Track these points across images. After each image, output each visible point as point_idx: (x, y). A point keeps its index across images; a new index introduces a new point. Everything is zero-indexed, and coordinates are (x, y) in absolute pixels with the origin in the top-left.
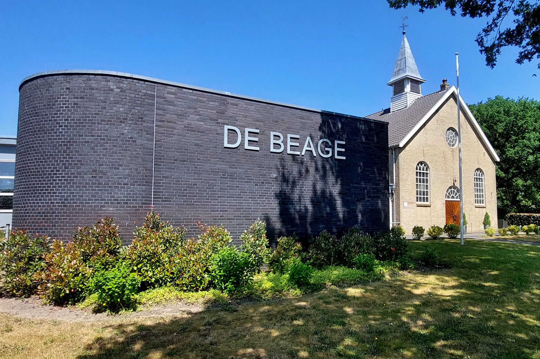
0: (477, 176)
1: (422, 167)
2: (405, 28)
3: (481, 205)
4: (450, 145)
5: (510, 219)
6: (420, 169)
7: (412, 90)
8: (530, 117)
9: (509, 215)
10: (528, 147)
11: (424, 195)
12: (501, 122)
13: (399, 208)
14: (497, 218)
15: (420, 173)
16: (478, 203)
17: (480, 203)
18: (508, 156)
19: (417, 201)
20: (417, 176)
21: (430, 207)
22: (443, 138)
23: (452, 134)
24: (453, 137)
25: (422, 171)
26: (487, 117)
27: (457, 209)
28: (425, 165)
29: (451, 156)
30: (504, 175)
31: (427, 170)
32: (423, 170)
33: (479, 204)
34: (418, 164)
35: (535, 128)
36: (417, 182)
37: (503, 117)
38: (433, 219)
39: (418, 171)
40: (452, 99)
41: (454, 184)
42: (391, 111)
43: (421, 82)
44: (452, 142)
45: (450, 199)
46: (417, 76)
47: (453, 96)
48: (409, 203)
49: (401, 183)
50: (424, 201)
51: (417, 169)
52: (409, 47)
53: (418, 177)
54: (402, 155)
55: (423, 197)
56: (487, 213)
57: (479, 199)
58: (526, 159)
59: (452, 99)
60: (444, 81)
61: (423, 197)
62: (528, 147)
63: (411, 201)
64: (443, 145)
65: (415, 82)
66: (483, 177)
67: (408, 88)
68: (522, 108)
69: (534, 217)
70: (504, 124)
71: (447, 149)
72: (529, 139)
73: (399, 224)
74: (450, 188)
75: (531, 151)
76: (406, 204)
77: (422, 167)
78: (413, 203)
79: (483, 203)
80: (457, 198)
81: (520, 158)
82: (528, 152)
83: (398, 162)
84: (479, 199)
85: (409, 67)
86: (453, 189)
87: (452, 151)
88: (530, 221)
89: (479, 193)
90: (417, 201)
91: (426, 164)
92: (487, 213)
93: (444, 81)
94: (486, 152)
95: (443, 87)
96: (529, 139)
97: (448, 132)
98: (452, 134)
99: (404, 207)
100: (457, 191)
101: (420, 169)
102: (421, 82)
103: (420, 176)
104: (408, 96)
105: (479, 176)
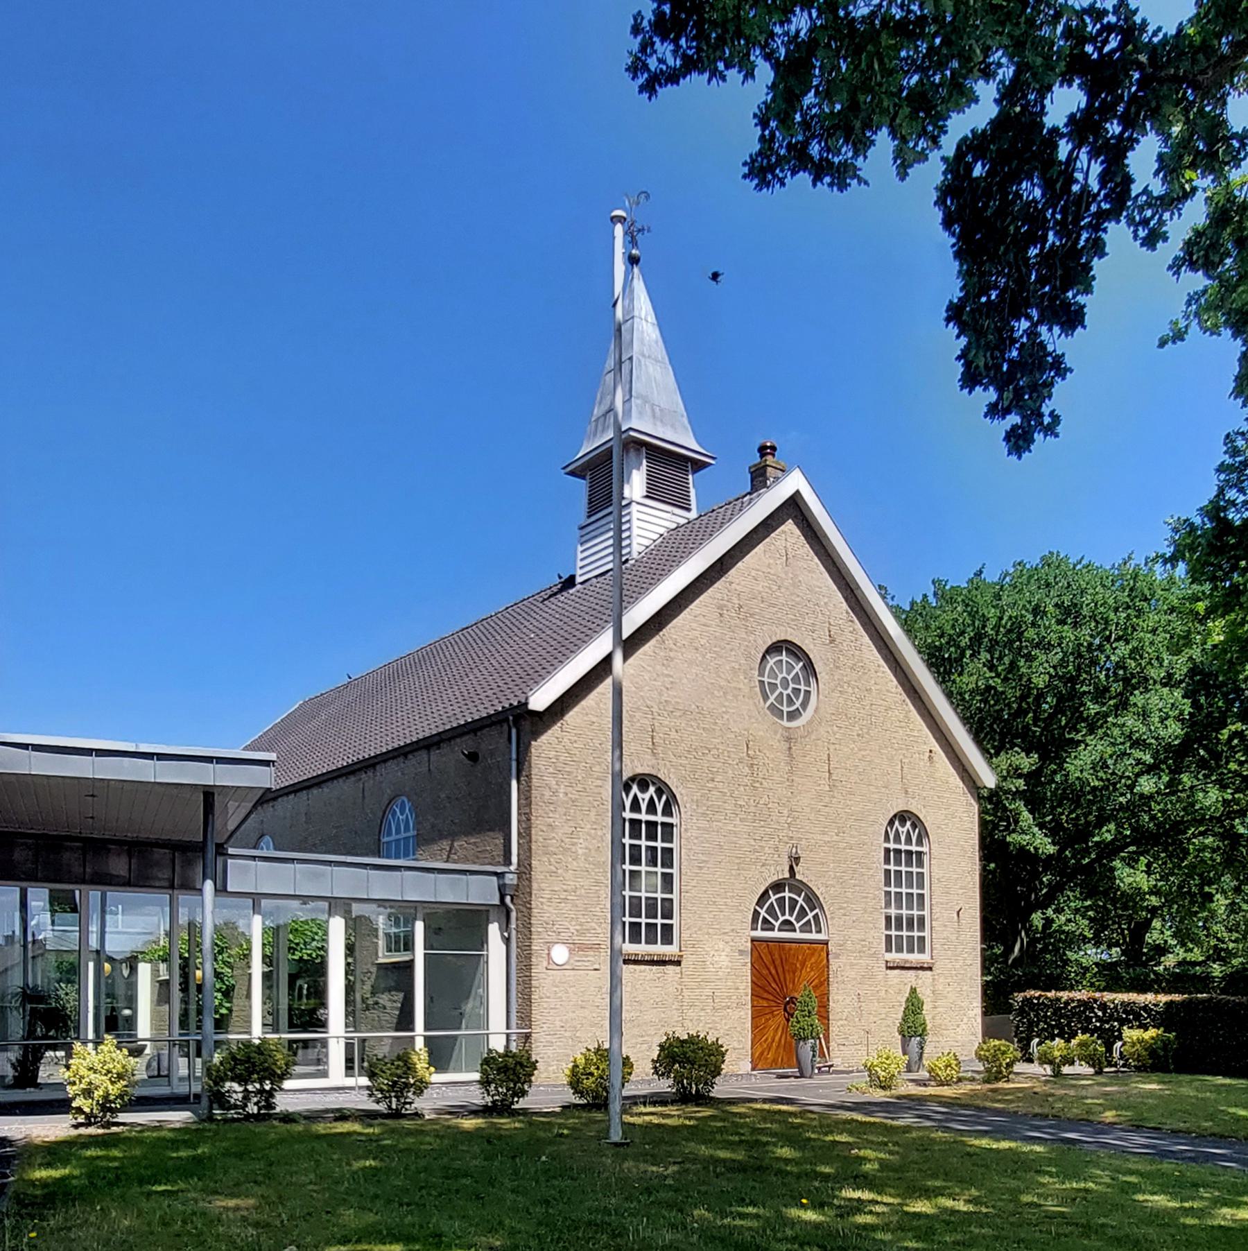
0: (897, 839)
1: (644, 798)
2: (639, 237)
3: (915, 958)
4: (775, 711)
5: (1021, 1012)
6: (897, 839)
7: (653, 493)
8: (1154, 631)
9: (1019, 997)
10: (1138, 743)
11: (652, 914)
12: (1048, 647)
13: (529, 967)
14: (978, 1011)
15: (898, 852)
16: (900, 950)
17: (911, 950)
18: (1071, 779)
19: (889, 950)
20: (887, 861)
21: (678, 963)
22: (747, 684)
23: (790, 668)
24: (796, 679)
25: (645, 819)
26: (996, 628)
27: (807, 975)
28: (659, 792)
29: (783, 757)
30: (1051, 849)
31: (919, 843)
32: (651, 808)
33: (905, 956)
34: (891, 823)
35: (1170, 676)
36: (888, 883)
37: (1051, 629)
38: (690, 1013)
39: (892, 846)
40: (790, 526)
41: (791, 869)
42: (579, 580)
43: (698, 466)
44: (790, 702)
45: (776, 934)
46: (684, 439)
47: (794, 508)
48: (577, 948)
49: (539, 865)
50: (651, 940)
51: (887, 839)
52: (652, 318)
53: (892, 867)
54: (545, 747)
55: (646, 924)
56: (913, 991)
57: (906, 930)
58: (1131, 788)
59: (790, 526)
60: (763, 450)
61: (646, 924)
62: (1138, 743)
63: (588, 939)
64: (748, 715)
65: (670, 468)
66: (925, 849)
67: (636, 484)
68: (1124, 597)
69: (1103, 1007)
70: (1056, 656)
71: (766, 729)
72: (1144, 715)
73: (527, 1037)
74: (778, 887)
75: (1148, 758)
76: (560, 954)
77: (644, 798)
78: (596, 947)
79: (922, 950)
80: (806, 928)
81: (1110, 785)
82: (1139, 762)
83: (529, 776)
84: (906, 930)
85: (645, 400)
86: (787, 894)
87: (788, 739)
88: (1089, 1020)
89: (904, 912)
90: (889, 950)
91: (917, 823)
92: (913, 991)
93: (763, 450)
94: (937, 748)
95: (759, 479)
96: (1144, 715)
97: (771, 661)
98: (785, 668)
99: (552, 965)
100: (808, 899)
101: (635, 806)
102: (698, 466)
103: (898, 863)
104: (635, 515)
105: (909, 840)
